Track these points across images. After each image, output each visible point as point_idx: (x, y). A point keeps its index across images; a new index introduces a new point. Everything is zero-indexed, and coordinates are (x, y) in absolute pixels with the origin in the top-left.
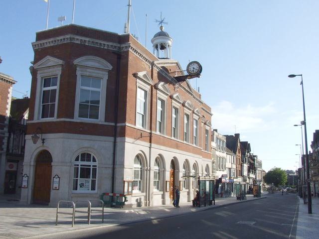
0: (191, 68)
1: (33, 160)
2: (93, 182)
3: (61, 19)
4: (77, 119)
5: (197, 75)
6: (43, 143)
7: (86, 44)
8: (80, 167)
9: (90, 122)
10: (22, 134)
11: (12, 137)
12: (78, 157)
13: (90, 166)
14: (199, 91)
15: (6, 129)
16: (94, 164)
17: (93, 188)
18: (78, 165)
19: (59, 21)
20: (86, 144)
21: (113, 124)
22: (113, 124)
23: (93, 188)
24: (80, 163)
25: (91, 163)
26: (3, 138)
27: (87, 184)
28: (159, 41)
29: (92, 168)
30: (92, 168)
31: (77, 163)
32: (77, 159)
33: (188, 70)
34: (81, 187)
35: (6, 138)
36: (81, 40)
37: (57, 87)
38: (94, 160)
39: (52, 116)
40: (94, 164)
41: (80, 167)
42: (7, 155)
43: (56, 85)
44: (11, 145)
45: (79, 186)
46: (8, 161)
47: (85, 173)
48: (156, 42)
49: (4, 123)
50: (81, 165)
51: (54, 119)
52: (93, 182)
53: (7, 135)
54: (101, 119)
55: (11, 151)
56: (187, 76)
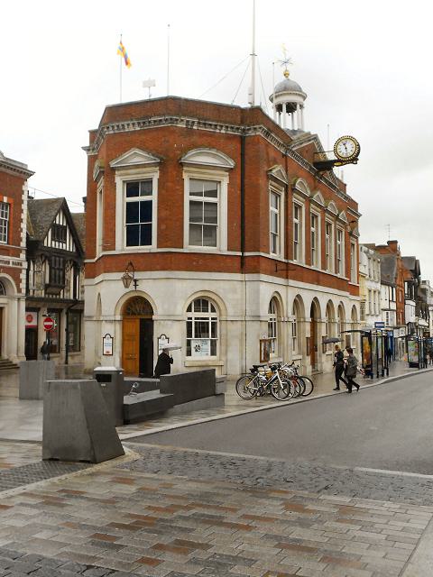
0: (341, 149)
1: (119, 311)
2: (213, 344)
3: (150, 84)
4: (188, 248)
5: (354, 159)
6: (136, 285)
7: (195, 128)
8: (193, 321)
9: (102, 221)
10: (45, 261)
11: (32, 268)
12: (190, 306)
13: (208, 319)
14: (342, 177)
15: (23, 256)
16: (214, 315)
17: (213, 353)
18: (191, 319)
19: (144, 86)
20: (199, 286)
21: (247, 254)
22: (247, 254)
23: (213, 353)
24: (193, 314)
25: (209, 315)
26: (20, 271)
27: (205, 347)
28: (284, 99)
29: (210, 321)
30: (210, 321)
31: (190, 315)
32: (189, 310)
33: (335, 151)
34: (196, 351)
35: (24, 272)
36: (188, 121)
37: (154, 198)
38: (213, 310)
39: (147, 241)
40: (214, 315)
41: (193, 321)
42: (26, 300)
43: (150, 193)
44: (31, 282)
45: (193, 350)
46: (28, 309)
47: (201, 329)
48: (277, 101)
49: (19, 245)
50: (196, 319)
51: (153, 247)
52: (213, 344)
53: (25, 265)
54: (222, 246)
55: (31, 294)
56: (335, 161)
